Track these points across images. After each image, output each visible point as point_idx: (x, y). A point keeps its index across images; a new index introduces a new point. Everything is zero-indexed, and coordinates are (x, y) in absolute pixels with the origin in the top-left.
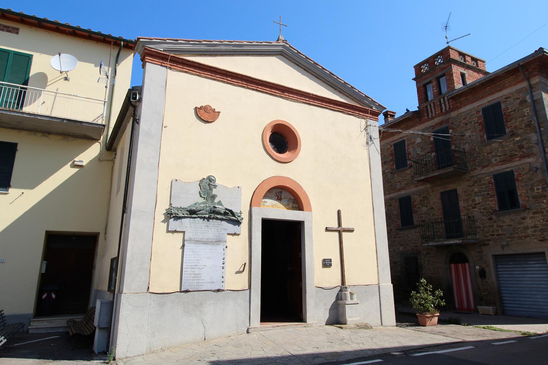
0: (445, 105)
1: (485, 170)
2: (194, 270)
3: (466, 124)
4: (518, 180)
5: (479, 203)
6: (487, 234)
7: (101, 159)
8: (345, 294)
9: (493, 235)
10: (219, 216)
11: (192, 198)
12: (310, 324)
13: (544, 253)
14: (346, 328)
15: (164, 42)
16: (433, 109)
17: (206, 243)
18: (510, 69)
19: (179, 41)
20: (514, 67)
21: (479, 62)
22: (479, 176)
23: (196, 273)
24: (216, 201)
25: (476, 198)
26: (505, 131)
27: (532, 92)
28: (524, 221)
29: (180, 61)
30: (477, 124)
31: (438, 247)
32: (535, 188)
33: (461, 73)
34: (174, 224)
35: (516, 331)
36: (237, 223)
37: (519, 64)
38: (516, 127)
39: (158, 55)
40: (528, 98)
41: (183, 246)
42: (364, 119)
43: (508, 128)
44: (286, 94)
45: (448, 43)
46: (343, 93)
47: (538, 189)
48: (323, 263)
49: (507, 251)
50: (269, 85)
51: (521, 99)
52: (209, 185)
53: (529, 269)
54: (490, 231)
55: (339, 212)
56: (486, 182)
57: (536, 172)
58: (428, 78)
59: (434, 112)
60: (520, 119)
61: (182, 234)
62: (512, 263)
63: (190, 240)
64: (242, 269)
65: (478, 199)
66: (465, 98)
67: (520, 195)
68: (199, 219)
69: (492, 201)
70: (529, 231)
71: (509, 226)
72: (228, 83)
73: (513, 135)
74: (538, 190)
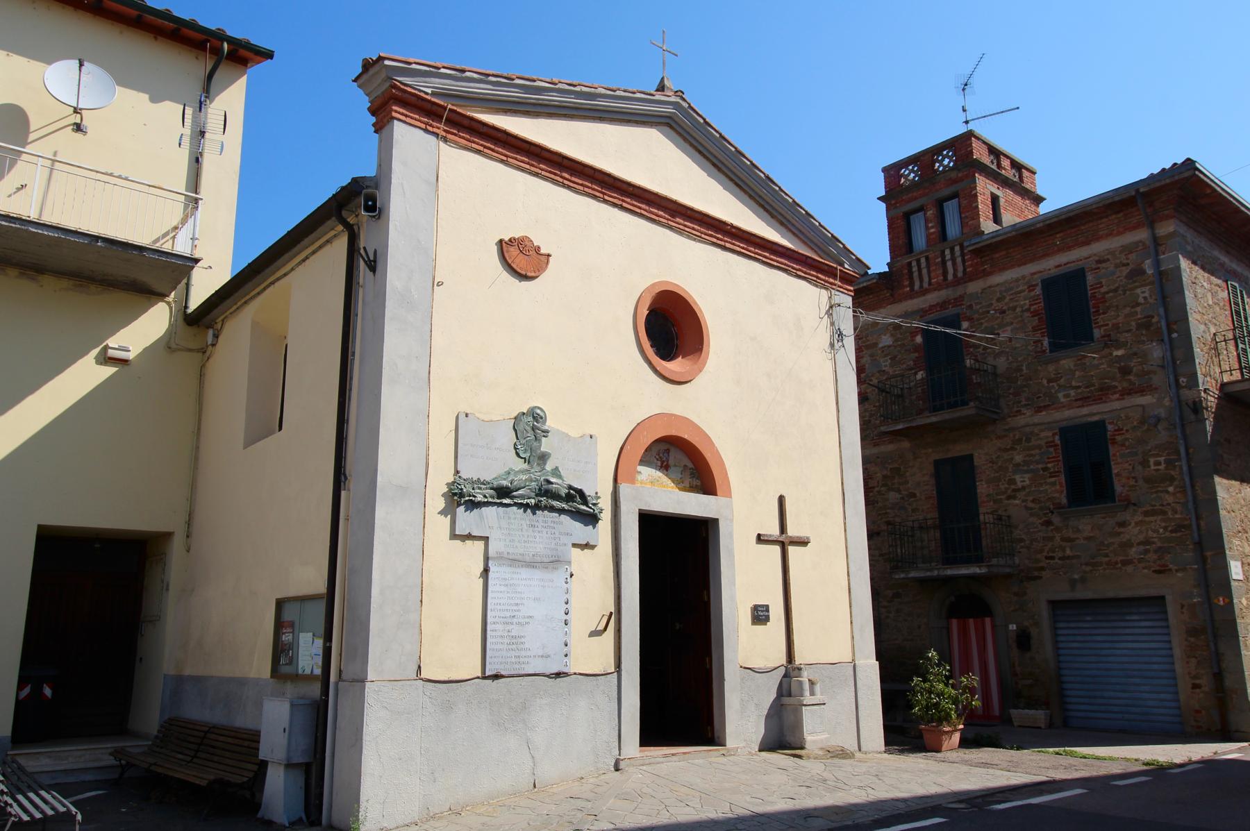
0: (954, 264)
1: (1043, 417)
2: (510, 627)
3: (1003, 312)
4: (1114, 442)
5: (1024, 488)
6: (1039, 556)
7: (173, 346)
8: (801, 683)
9: (1052, 558)
10: (556, 504)
11: (496, 461)
13: (1163, 598)
14: (809, 758)
15: (434, 72)
16: (925, 271)
17: (531, 565)
18: (1117, 199)
19: (468, 74)
20: (1125, 196)
21: (1025, 173)
22: (1028, 429)
24: (549, 467)
25: (1018, 478)
26: (1092, 334)
27: (1157, 254)
28: (1122, 530)
29: (466, 122)
30: (1027, 314)
31: (922, 581)
32: (1152, 460)
33: (992, 194)
34: (467, 520)
35: (1127, 760)
36: (591, 519)
37: (1137, 191)
38: (1116, 327)
39: (420, 103)
40: (1148, 266)
41: (486, 571)
42: (826, 289)
43: (1099, 327)
44: (678, 220)
45: (967, 122)
46: (786, 227)
47: (1158, 463)
49: (1080, 594)
50: (647, 196)
51: (1131, 266)
52: (534, 429)
53: (1127, 631)
54: (1047, 549)
55: (781, 500)
56: (1043, 443)
57: (1156, 426)
58: (916, 198)
59: (926, 279)
60: (1127, 310)
61: (481, 544)
62: (1089, 618)
63: (500, 557)
64: (601, 627)
65: (1022, 480)
66: (1004, 253)
67: (1118, 475)
69: (1054, 484)
70: (1133, 552)
71: (1088, 539)
72: (564, 186)
73: (1110, 342)
74: (1158, 464)
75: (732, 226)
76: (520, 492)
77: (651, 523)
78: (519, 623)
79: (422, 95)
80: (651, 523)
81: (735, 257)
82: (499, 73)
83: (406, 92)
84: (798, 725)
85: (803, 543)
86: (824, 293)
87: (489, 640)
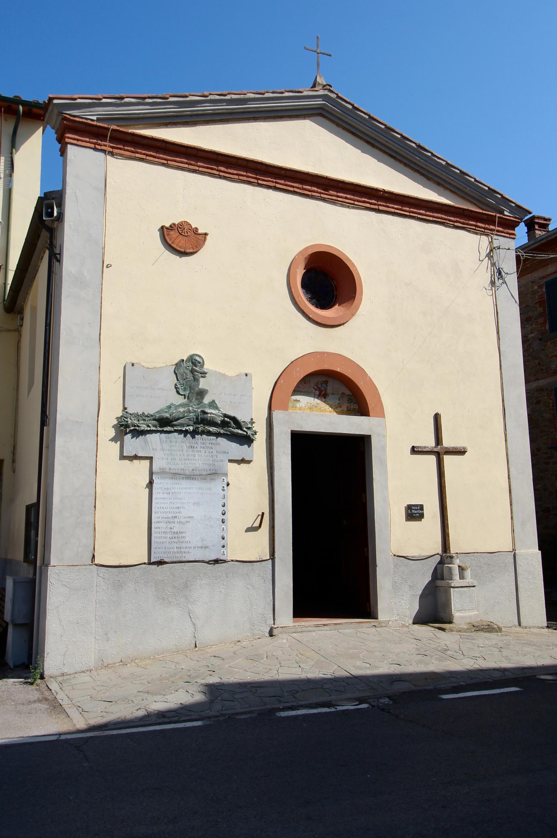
2: (172, 525)
8: (450, 569)
10: (212, 429)
11: (163, 397)
12: (384, 622)
17: (190, 477)
19: (126, 100)
29: (129, 138)
34: (132, 445)
41: (150, 484)
42: (487, 235)
44: (331, 192)
46: (443, 187)
52: (192, 371)
55: (437, 418)
61: (147, 462)
63: (163, 473)
64: (257, 524)
68: (176, 434)
72: (220, 177)
75: (384, 191)
76: (180, 421)
77: (302, 442)
78: (180, 522)
80: (302, 442)
81: (390, 217)
82: (154, 95)
83: (75, 121)
84: (447, 604)
85: (461, 452)
86: (485, 240)
87: (154, 535)
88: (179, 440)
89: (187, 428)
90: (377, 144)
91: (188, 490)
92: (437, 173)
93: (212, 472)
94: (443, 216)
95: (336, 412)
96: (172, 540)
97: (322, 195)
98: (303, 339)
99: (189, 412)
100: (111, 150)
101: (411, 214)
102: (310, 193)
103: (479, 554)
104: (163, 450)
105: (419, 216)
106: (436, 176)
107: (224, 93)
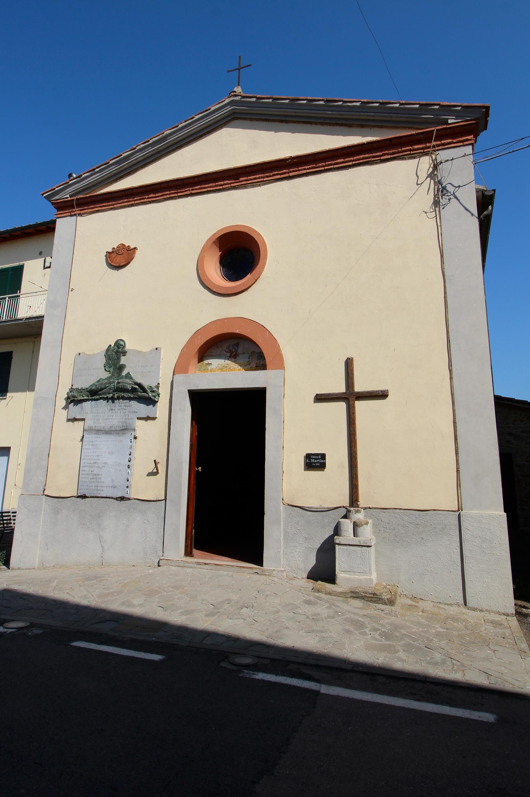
2: (93, 469)
10: (126, 395)
11: (98, 374)
12: (267, 570)
17: (108, 432)
19: (83, 176)
23: (95, 472)
24: (124, 373)
29: (89, 200)
34: (75, 410)
36: (151, 402)
41: (83, 437)
42: (427, 154)
44: (241, 179)
48: (305, 461)
68: (102, 401)
75: (292, 158)
76: (103, 391)
78: (98, 467)
79: (66, 199)
80: (199, 399)
82: (100, 164)
88: (103, 405)
89: (108, 395)
90: (288, 119)
91: (105, 443)
92: (355, 117)
93: (123, 428)
94: (367, 155)
95: (245, 370)
96: (92, 480)
97: (232, 185)
98: (213, 311)
99: (110, 383)
100: (80, 212)
101: (326, 168)
102: (221, 187)
103: (402, 511)
104: (92, 413)
105: (335, 166)
106: (357, 119)
107: (147, 140)
